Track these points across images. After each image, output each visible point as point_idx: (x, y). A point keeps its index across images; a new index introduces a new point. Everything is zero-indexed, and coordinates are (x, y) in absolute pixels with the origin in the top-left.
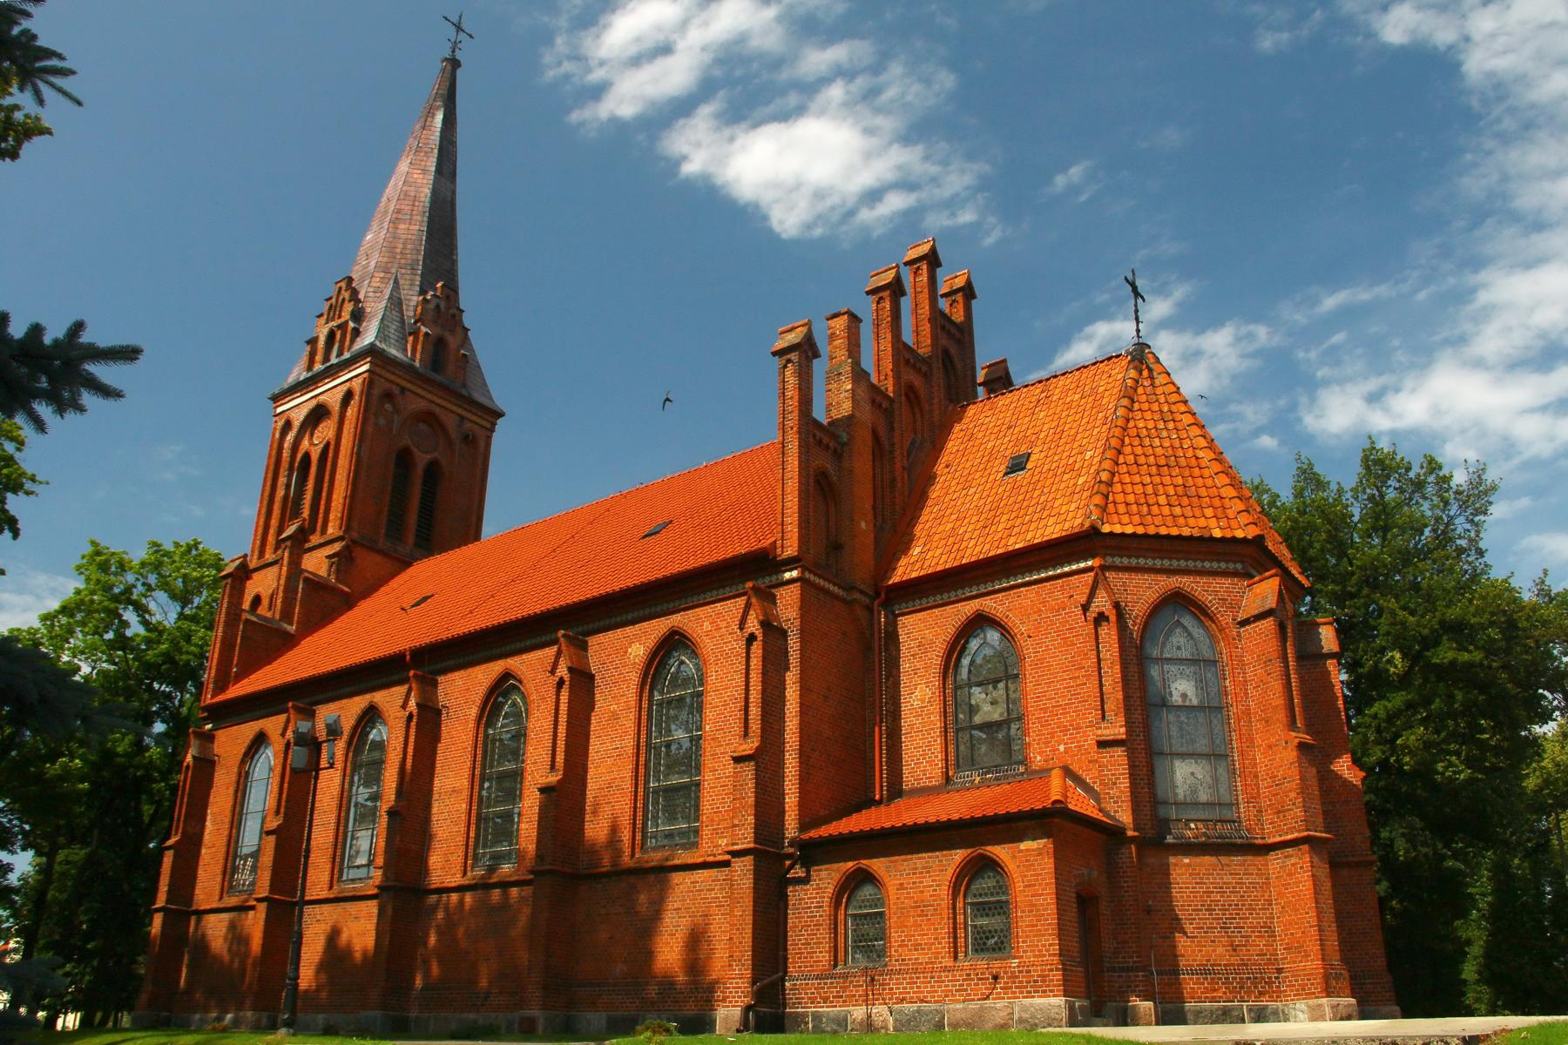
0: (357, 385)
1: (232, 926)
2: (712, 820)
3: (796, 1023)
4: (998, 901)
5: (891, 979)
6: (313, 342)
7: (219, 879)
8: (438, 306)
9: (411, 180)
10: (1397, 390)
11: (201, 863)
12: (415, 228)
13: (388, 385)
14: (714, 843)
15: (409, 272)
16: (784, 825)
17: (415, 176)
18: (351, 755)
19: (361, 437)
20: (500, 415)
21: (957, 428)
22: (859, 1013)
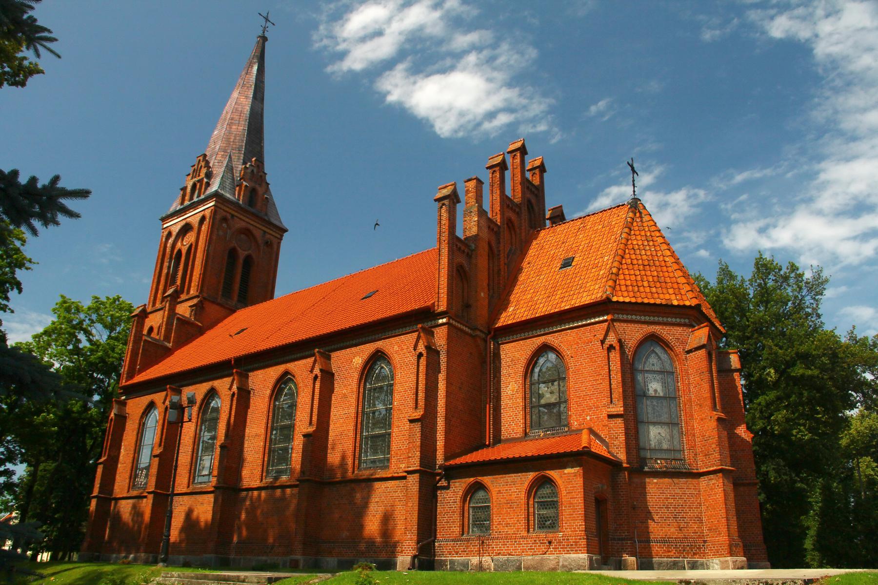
0: (208, 213)
1: (134, 507)
2: (397, 454)
3: (441, 565)
4: (552, 501)
5: (493, 542)
6: (184, 189)
7: (127, 481)
8: (252, 171)
9: (239, 102)
10: (775, 226)
11: (118, 472)
12: (241, 128)
13: (224, 213)
14: (398, 466)
15: (237, 152)
16: (436, 457)
17: (242, 100)
18: (200, 414)
19: (210, 242)
20: (286, 231)
21: (534, 242)
22: (475, 560)
